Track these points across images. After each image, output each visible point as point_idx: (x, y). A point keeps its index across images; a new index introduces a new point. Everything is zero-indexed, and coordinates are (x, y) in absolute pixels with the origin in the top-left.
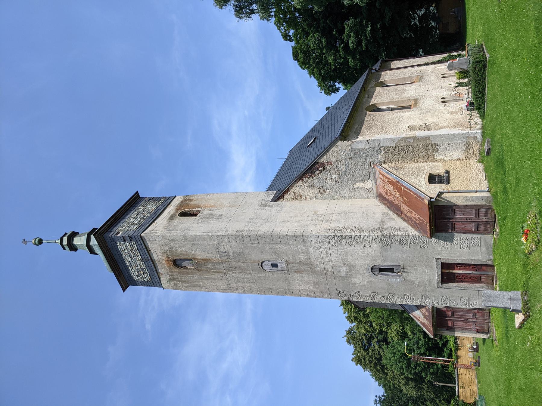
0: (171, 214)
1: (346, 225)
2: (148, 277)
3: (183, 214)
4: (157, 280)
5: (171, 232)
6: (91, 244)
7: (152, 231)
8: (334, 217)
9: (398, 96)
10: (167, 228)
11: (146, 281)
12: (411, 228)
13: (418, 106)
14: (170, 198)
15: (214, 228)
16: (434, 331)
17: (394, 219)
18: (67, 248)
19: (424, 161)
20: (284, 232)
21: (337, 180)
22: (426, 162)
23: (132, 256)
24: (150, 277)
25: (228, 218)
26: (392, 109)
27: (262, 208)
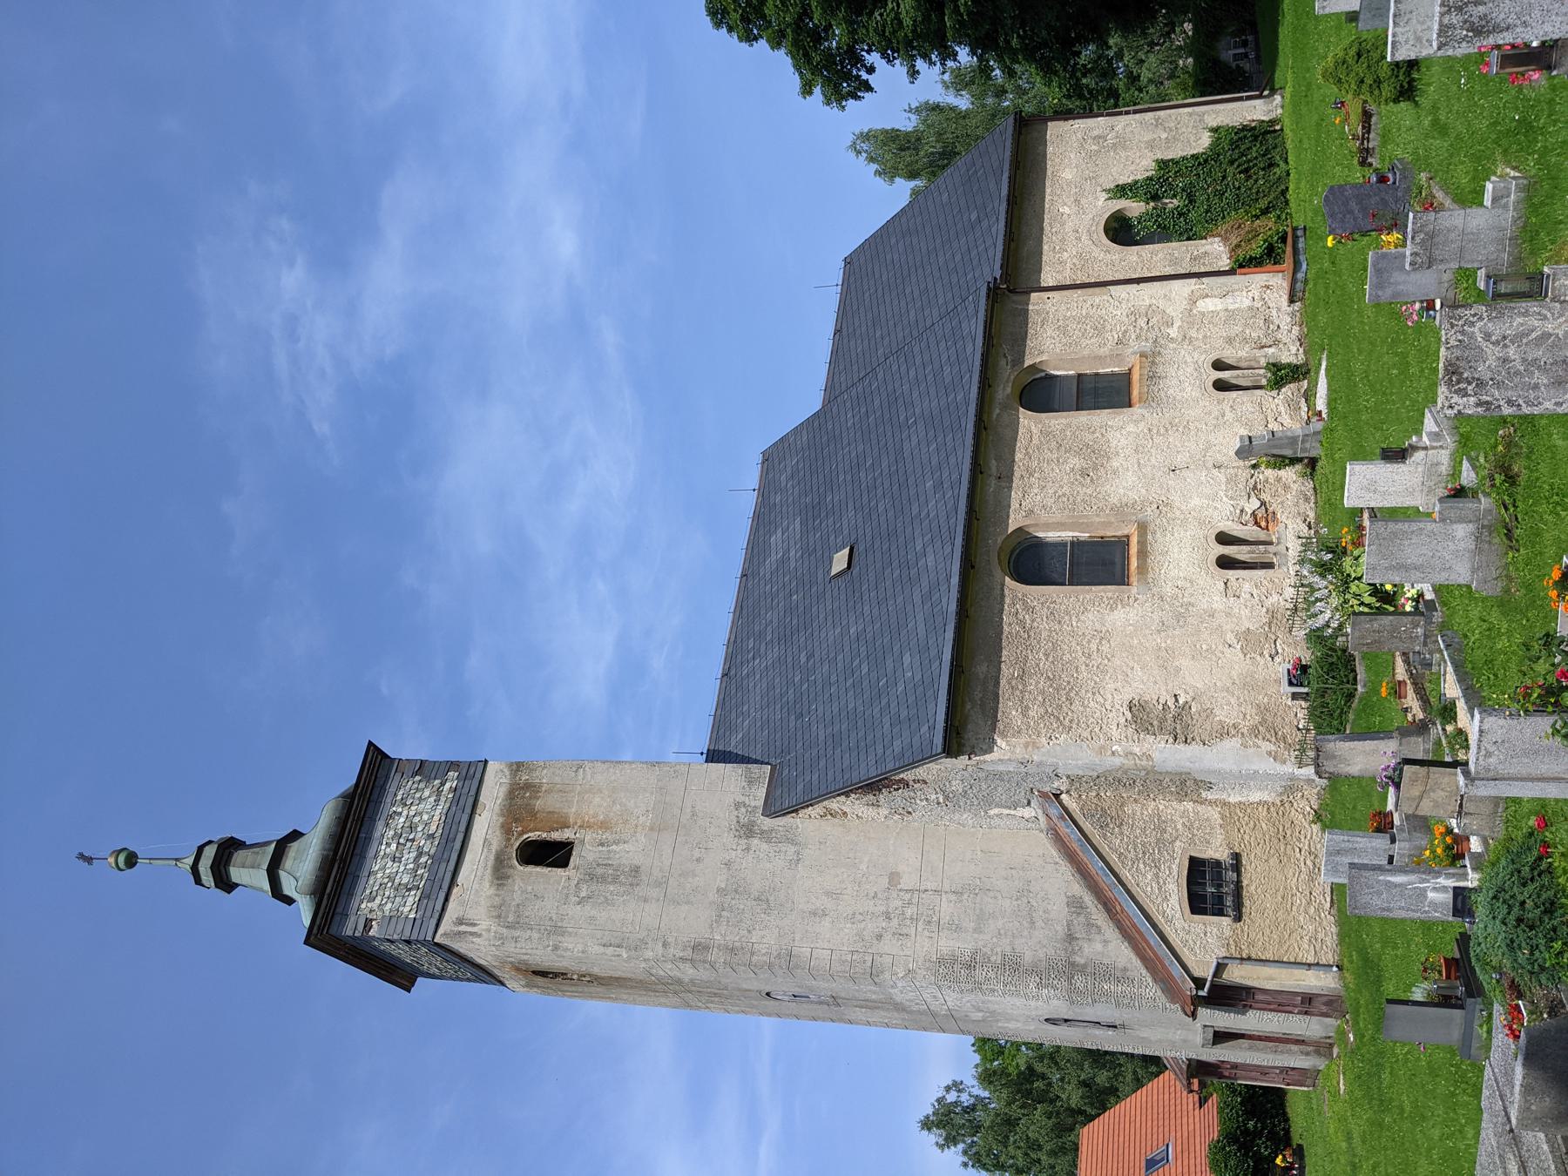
12: (1144, 972)
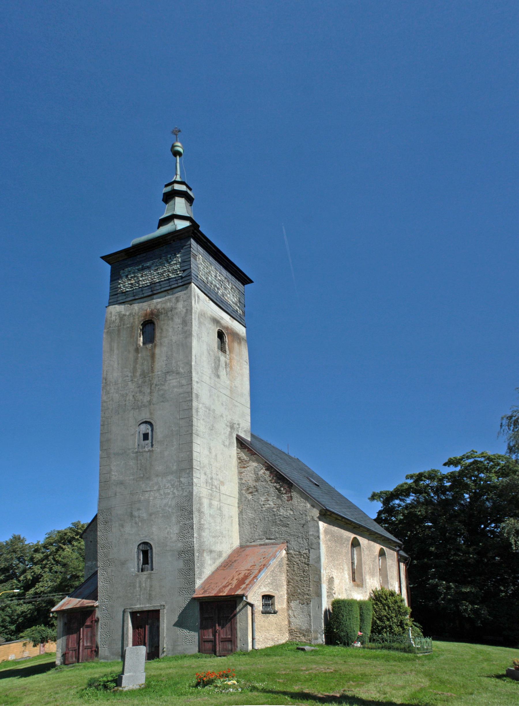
0: (221, 320)
1: (206, 515)
2: (124, 289)
3: (221, 335)
4: (120, 299)
5: (197, 319)
6: (177, 221)
7: (198, 297)
8: (215, 503)
9: (367, 569)
10: (202, 315)
11: (119, 286)
13: (354, 587)
14: (242, 320)
15: (201, 369)
16: (13, 642)
17: (214, 563)
18: (169, 189)
19: (289, 591)
20: (196, 448)
21: (266, 506)
22: (288, 594)
23: (159, 271)
24: (125, 291)
25: (215, 385)
26: (353, 563)
27: (228, 424)
